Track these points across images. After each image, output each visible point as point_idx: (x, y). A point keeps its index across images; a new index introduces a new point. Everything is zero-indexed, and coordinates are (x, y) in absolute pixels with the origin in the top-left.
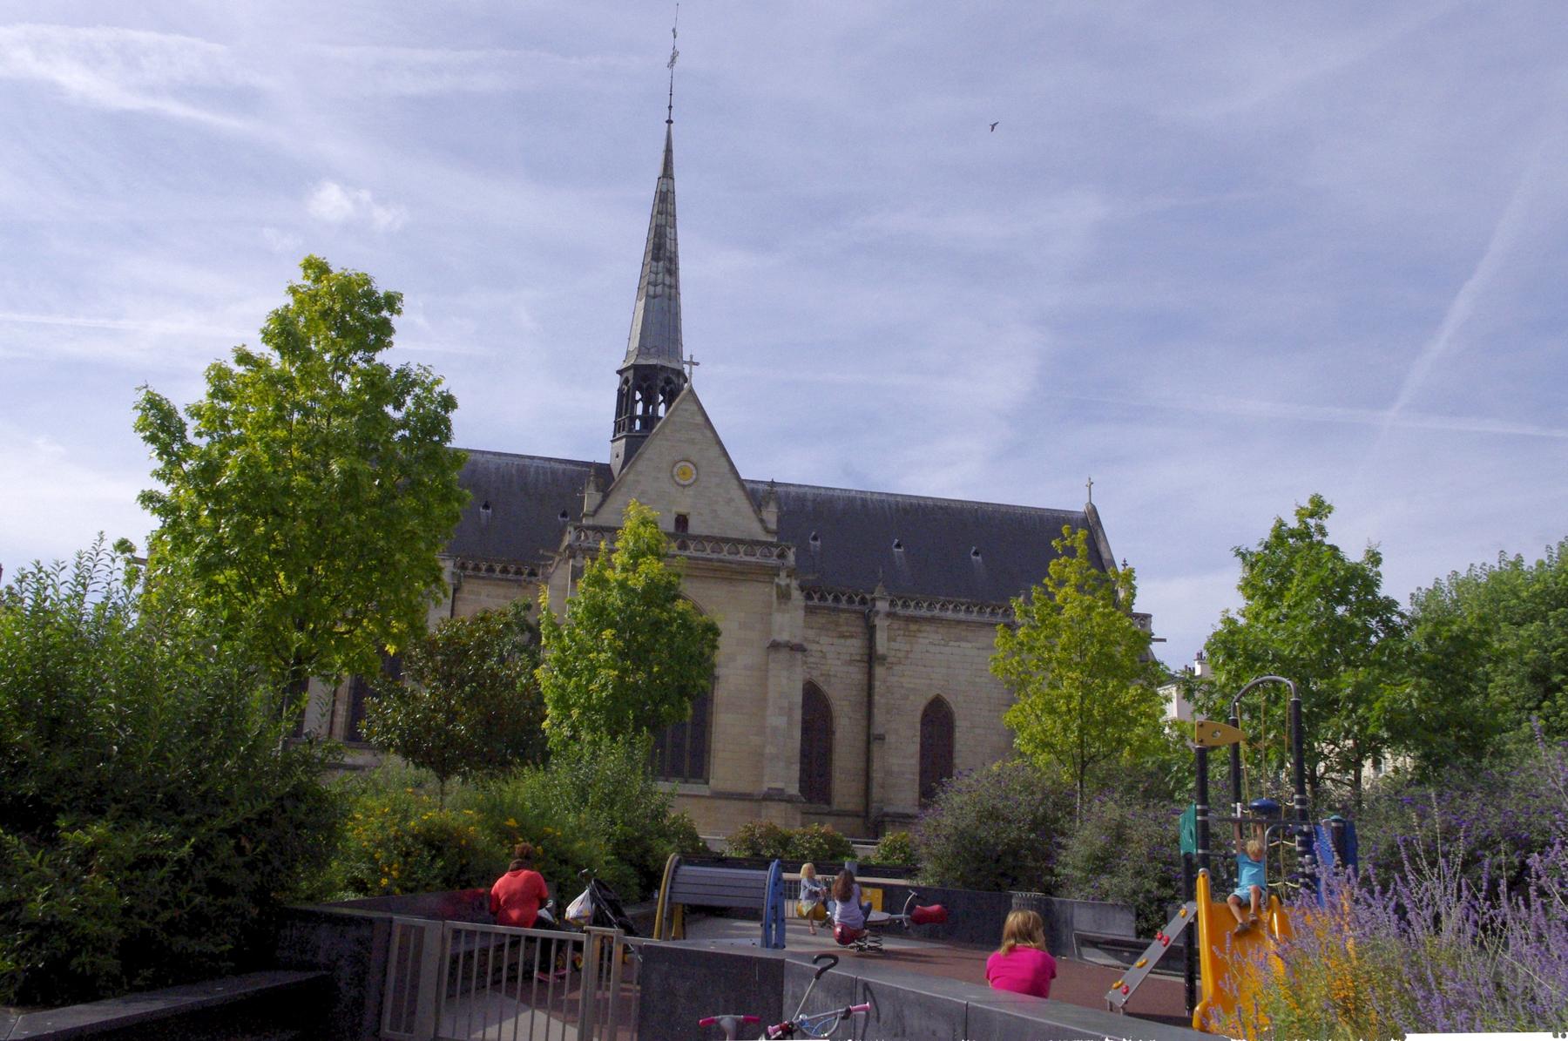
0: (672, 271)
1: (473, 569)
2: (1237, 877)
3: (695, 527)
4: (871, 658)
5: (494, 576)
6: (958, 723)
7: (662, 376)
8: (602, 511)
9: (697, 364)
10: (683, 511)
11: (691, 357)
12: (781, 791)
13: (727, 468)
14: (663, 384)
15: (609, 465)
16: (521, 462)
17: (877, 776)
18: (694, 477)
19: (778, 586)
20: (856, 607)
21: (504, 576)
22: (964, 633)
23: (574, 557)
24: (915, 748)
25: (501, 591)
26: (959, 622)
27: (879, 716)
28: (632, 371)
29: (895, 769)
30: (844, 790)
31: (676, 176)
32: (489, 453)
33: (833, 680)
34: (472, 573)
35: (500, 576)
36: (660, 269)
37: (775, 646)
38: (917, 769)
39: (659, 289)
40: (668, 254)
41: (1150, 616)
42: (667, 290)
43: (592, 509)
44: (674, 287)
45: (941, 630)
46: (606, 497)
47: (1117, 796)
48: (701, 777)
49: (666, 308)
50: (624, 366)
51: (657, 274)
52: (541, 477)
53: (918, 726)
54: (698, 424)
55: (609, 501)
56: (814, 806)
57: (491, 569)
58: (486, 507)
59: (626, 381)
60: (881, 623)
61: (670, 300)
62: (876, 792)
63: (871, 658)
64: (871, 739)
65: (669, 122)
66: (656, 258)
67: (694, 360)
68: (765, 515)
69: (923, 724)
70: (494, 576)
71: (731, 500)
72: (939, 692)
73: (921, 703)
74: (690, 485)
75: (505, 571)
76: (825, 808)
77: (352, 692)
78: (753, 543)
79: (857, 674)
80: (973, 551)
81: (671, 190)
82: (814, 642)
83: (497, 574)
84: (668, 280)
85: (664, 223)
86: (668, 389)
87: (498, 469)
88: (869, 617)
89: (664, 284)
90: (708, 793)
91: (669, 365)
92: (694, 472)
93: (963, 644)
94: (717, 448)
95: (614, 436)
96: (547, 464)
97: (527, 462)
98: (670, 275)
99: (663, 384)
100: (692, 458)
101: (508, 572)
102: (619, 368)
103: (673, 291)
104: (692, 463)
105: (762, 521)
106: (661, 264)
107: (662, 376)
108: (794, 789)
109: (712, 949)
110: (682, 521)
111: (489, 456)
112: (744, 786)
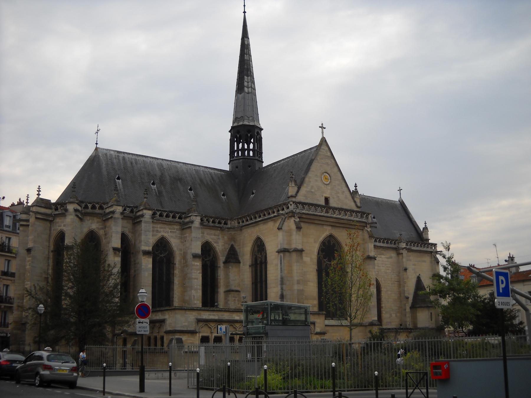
3: (333, 203)
8: (298, 194)
9: (325, 128)
10: (327, 196)
13: (340, 177)
22: (382, 252)
41: (436, 244)
43: (294, 194)
46: (299, 188)
52: (206, 175)
54: (328, 156)
68: (356, 199)
78: (352, 211)
87: (187, 170)
104: (328, 174)
105: (355, 202)
110: (327, 200)
111: (181, 164)
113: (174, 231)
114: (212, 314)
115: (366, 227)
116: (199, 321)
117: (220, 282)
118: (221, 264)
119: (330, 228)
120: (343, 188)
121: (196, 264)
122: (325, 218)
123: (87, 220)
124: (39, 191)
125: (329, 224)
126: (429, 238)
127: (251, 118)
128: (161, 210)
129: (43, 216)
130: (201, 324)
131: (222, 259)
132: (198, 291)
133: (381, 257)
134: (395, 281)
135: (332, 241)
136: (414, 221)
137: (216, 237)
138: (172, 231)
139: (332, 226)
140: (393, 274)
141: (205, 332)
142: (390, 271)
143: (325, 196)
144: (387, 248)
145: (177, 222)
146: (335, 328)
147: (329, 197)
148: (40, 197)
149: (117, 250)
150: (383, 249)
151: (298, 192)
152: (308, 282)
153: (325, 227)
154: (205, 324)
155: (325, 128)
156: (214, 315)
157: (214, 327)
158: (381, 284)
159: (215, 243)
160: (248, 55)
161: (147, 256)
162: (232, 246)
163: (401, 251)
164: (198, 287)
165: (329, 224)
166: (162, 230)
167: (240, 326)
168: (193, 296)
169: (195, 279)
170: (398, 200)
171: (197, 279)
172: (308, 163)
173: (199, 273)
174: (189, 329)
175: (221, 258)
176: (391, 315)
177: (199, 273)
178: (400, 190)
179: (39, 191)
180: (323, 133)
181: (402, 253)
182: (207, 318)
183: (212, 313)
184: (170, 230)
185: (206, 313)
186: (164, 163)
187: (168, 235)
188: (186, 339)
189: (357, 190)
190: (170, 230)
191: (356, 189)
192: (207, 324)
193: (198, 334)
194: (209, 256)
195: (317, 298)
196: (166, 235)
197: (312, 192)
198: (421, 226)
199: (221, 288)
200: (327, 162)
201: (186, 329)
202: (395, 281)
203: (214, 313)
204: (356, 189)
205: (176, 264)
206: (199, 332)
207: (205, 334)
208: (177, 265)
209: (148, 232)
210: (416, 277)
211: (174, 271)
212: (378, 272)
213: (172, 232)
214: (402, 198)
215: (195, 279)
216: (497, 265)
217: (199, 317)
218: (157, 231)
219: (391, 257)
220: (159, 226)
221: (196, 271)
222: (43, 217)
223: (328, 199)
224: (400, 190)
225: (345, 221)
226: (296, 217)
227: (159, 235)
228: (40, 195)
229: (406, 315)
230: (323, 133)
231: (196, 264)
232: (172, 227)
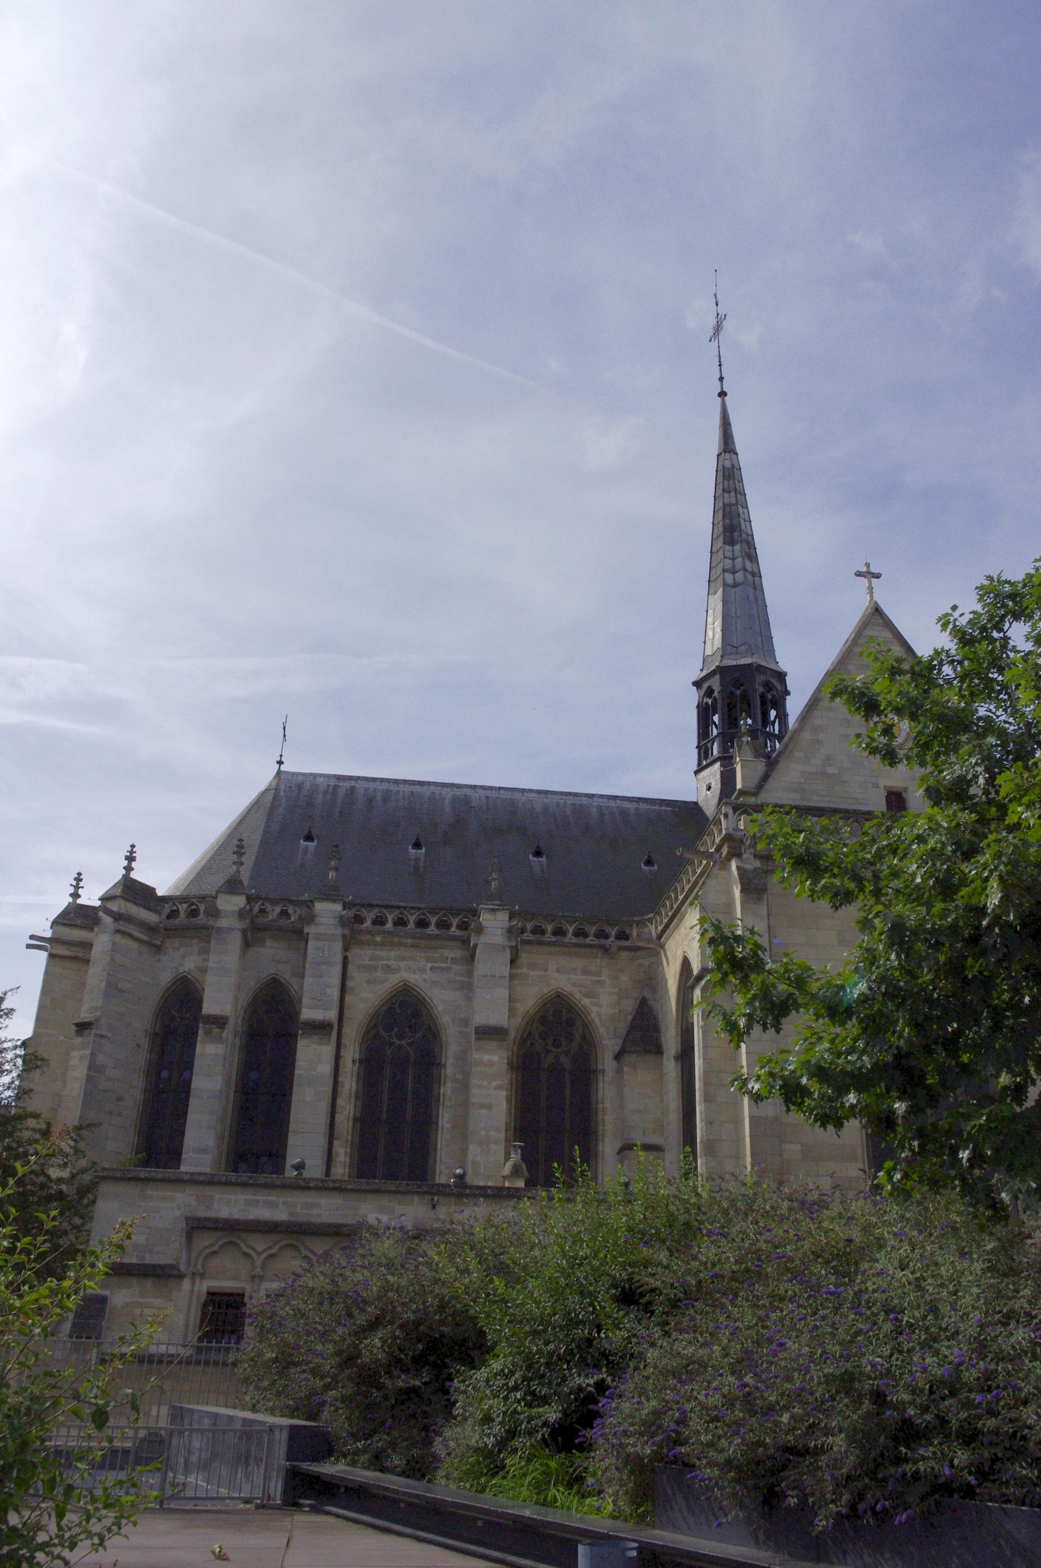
0: (751, 555)
2: (642, 1459)
5: (566, 940)
7: (760, 678)
8: (767, 786)
9: (878, 576)
11: (868, 565)
14: (761, 689)
15: (696, 803)
16: (577, 801)
21: (581, 940)
23: (739, 855)
25: (579, 963)
28: (718, 677)
31: (738, 449)
32: (531, 791)
34: (532, 937)
35: (574, 940)
36: (737, 553)
39: (740, 576)
40: (744, 536)
42: (750, 577)
43: (752, 784)
44: (757, 574)
47: (907, 1377)
49: (751, 598)
50: (704, 673)
51: (733, 559)
55: (774, 775)
57: (559, 932)
58: (538, 853)
59: (709, 692)
61: (755, 589)
65: (722, 394)
66: (730, 541)
67: (873, 570)
70: (566, 940)
75: (580, 933)
77: (358, 1125)
81: (736, 465)
83: (570, 937)
84: (748, 565)
85: (733, 501)
86: (769, 696)
89: (745, 570)
91: (763, 663)
95: (700, 763)
96: (612, 804)
97: (585, 801)
98: (751, 560)
99: (761, 689)
101: (585, 935)
102: (695, 678)
106: (737, 547)
107: (760, 678)
109: (743, 1549)
113: (444, 965)
114: (265, 1202)
116: (196, 1226)
117: (603, 1120)
118: (607, 1062)
121: (486, 1057)
123: (174, 948)
124: (77, 887)
127: (742, 648)
128: (399, 907)
129: (73, 949)
130: (204, 1241)
131: (608, 1043)
132: (492, 1146)
137: (590, 978)
138: (437, 965)
143: (885, 787)
145: (454, 938)
147: (906, 789)
148: (79, 901)
149: (213, 1023)
151: (766, 777)
154: (284, 1243)
155: (878, 576)
156: (268, 1204)
157: (264, 1255)
159: (586, 996)
160: (733, 494)
161: (317, 1037)
162: (643, 1003)
164: (493, 1133)
166: (402, 964)
167: (270, 1248)
169: (482, 1106)
171: (489, 1107)
172: (720, 646)
173: (499, 1087)
174: (148, 1260)
175: (606, 1042)
177: (499, 1087)
179: (77, 887)
180: (871, 589)
182: (236, 1216)
183: (262, 1197)
184: (429, 965)
185: (233, 1197)
186: (475, 795)
187: (424, 980)
188: (127, 1300)
190: (429, 965)
193: (186, 1284)
194: (570, 1037)
196: (413, 978)
199: (606, 1140)
201: (134, 1261)
203: (273, 1197)
205: (445, 1065)
206: (193, 1274)
208: (449, 1071)
209: (324, 967)
211: (439, 1088)
213: (437, 968)
215: (482, 1106)
217: (202, 1213)
218: (389, 969)
220: (393, 954)
221: (485, 1083)
222: (67, 953)
223: (904, 795)
226: (744, 856)
227: (394, 980)
228: (71, 895)
230: (871, 589)
231: (486, 1057)
232: (436, 955)
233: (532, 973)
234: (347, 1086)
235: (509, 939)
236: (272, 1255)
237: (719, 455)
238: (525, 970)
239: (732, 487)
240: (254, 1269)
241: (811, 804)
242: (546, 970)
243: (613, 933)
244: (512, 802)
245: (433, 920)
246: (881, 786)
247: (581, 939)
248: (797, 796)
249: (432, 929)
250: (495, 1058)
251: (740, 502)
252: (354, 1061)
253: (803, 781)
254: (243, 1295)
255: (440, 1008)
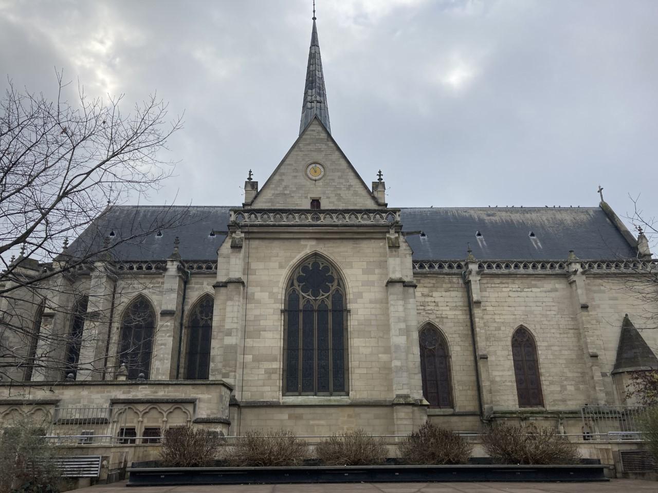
0: (321, 92)
1: (207, 268)
3: (325, 205)
4: (471, 305)
6: (538, 344)
10: (315, 195)
12: (406, 397)
17: (485, 384)
18: (322, 173)
19: (389, 239)
20: (455, 270)
22: (533, 282)
24: (510, 363)
26: (529, 275)
27: (481, 344)
29: (498, 379)
30: (463, 397)
31: (320, 45)
33: (445, 320)
34: (197, 271)
36: (314, 93)
37: (391, 283)
38: (514, 378)
45: (516, 282)
48: (343, 390)
53: (511, 348)
56: (442, 410)
60: (474, 279)
62: (486, 396)
63: (471, 305)
64: (478, 359)
65: (314, 19)
69: (513, 345)
71: (350, 186)
72: (522, 323)
73: (510, 332)
74: (320, 179)
76: (450, 411)
79: (460, 315)
80: (530, 234)
82: (428, 296)
88: (465, 276)
90: (349, 401)
92: (322, 170)
93: (534, 290)
94: (337, 153)
100: (320, 162)
103: (322, 105)
108: (417, 394)
110: (316, 203)
112: (379, 394)
113: (158, 285)
115: (389, 232)
116: (114, 402)
119: (313, 243)
120: (350, 181)
122: (299, 228)
125: (308, 237)
126: (651, 253)
130: (116, 408)
133: (531, 291)
134: (569, 329)
135: (322, 264)
136: (624, 231)
139: (317, 239)
140: (562, 317)
141: (130, 420)
142: (553, 313)
144: (543, 276)
146: (319, 410)
147: (320, 198)
150: (535, 277)
152: (261, 332)
153: (303, 242)
158: (536, 335)
163: (573, 278)
164: (166, 356)
165: (307, 236)
167: (170, 409)
168: (157, 368)
169: (162, 344)
170: (598, 206)
171: (165, 345)
176: (563, 388)
178: (600, 190)
181: (575, 281)
189: (382, 181)
191: (380, 179)
192: (155, 406)
195: (279, 357)
197: (285, 194)
198: (635, 235)
200: (320, 147)
202: (569, 329)
204: (380, 179)
207: (129, 425)
210: (622, 319)
212: (527, 315)
214: (604, 200)
215: (162, 344)
216: (307, 205)
219: (556, 290)
224: (600, 190)
225: (340, 228)
229: (594, 388)
232: (155, 281)
233: (196, 286)
234: (114, 338)
235: (178, 273)
236: (171, 412)
237: (311, 48)
238: (193, 285)
239: (314, 63)
240: (187, 418)
241: (275, 208)
242: (203, 284)
243: (204, 267)
244: (210, 212)
245: (154, 266)
246: (309, 197)
247: (209, 270)
248: (270, 204)
249: (153, 270)
250: (169, 324)
251: (317, 69)
252: (118, 328)
253: (273, 197)
254: (135, 429)
255: (155, 304)
